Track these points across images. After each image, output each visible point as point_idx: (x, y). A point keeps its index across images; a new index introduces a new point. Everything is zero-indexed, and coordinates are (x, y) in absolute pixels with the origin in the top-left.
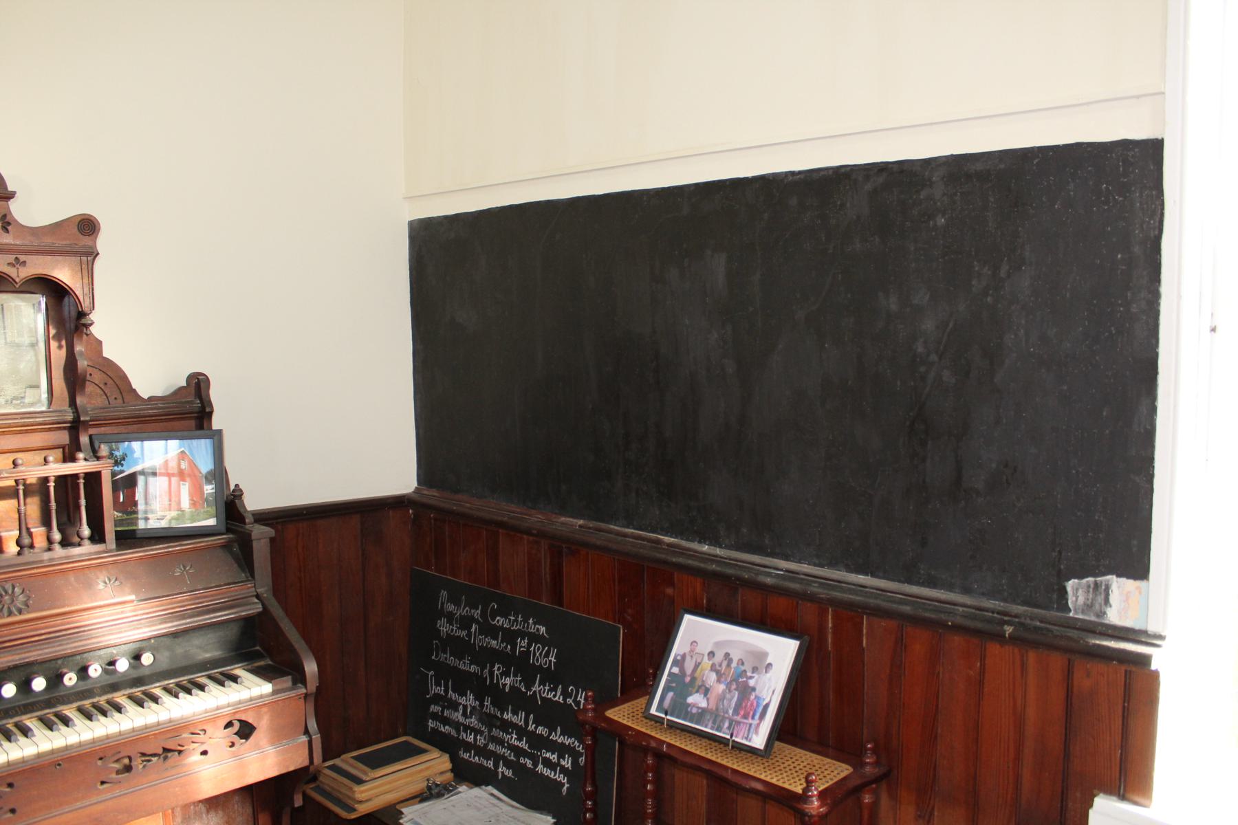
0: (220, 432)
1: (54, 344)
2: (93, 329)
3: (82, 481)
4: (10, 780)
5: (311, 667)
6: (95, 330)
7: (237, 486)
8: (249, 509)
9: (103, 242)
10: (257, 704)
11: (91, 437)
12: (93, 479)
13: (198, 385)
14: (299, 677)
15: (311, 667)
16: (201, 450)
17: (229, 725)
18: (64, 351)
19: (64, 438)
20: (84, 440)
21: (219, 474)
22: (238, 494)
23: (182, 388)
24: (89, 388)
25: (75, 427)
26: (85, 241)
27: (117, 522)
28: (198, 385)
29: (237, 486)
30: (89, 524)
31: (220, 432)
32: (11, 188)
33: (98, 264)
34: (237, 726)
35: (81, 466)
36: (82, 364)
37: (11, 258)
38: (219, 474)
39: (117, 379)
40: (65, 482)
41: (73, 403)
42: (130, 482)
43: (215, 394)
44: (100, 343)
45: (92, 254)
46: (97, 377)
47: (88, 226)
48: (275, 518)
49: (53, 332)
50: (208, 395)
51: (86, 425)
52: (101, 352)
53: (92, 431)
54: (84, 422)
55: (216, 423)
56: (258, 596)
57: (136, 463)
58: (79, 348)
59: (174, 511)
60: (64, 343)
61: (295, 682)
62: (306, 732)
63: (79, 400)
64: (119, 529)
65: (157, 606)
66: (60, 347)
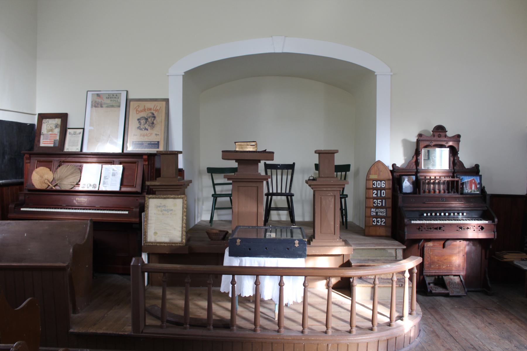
0: (481, 175)
1: (451, 157)
2: (458, 155)
3: (455, 182)
4: (444, 225)
5: (496, 220)
6: (459, 155)
7: (484, 186)
8: (488, 193)
9: (461, 139)
10: (486, 224)
11: (456, 175)
12: (457, 182)
13: (477, 166)
14: (493, 221)
15: (496, 220)
16: (477, 179)
17: (479, 226)
18: (453, 159)
19: (451, 174)
20: (455, 175)
21: (480, 183)
22: (484, 187)
23: (474, 167)
24: (457, 166)
25: (454, 173)
26: (458, 139)
27: (461, 191)
28: (477, 166)
29: (484, 186)
30: (456, 190)
31: (481, 175)
32: (447, 130)
33: (460, 143)
34: (481, 227)
35: (456, 179)
36: (456, 161)
37: (446, 142)
38: (480, 183)
39: (461, 164)
40: (453, 182)
41: (454, 168)
42: (463, 184)
43: (480, 168)
44: (459, 157)
45: (459, 141)
46: (458, 164)
47: (459, 136)
48: (494, 196)
49: (451, 155)
50: (479, 168)
51: (456, 172)
52: (459, 159)
53: (457, 174)
54: (456, 172)
55: (480, 174)
56: (487, 207)
57: (464, 180)
58: (455, 158)
59: (466, 182)
60: (453, 157)
61: (493, 222)
62: (494, 232)
63: (455, 168)
64: (455, 182)
65: (467, 205)
66: (452, 158)
